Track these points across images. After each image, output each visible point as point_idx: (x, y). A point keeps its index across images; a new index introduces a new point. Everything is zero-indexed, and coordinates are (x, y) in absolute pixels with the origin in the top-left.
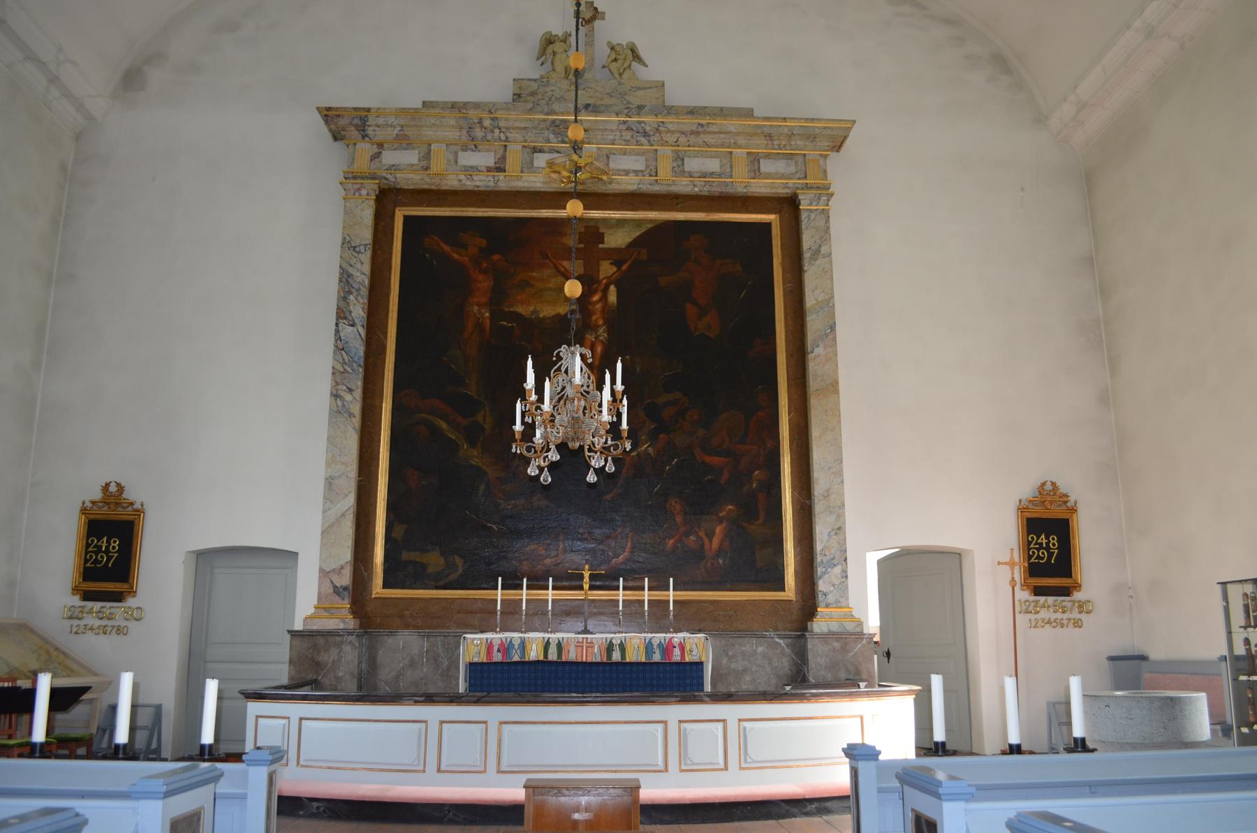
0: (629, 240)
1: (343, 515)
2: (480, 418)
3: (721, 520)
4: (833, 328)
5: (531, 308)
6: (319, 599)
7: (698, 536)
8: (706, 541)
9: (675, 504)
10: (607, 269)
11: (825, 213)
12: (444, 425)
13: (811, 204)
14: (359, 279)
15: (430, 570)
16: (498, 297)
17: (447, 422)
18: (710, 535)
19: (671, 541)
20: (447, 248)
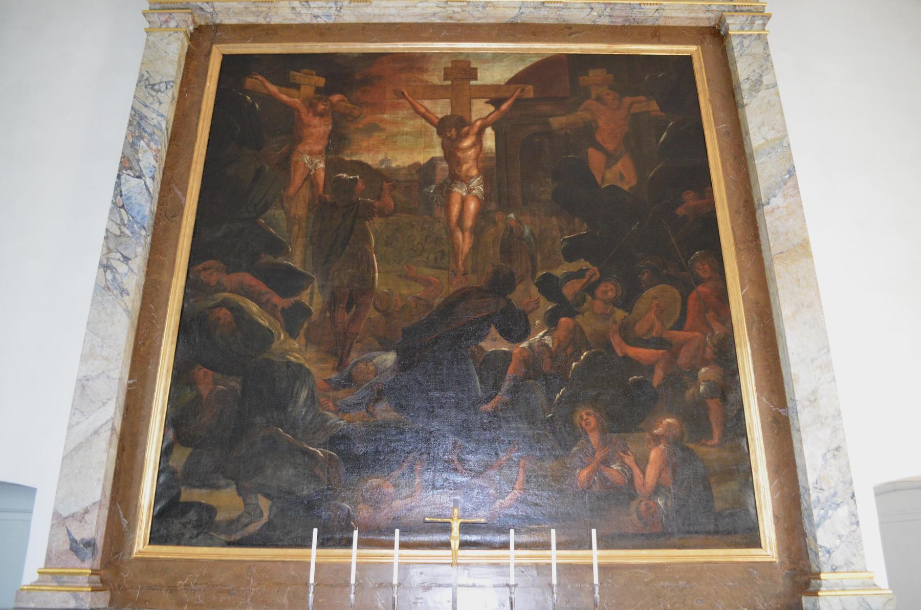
0: (509, 75)
1: (96, 432)
2: (304, 297)
3: (657, 439)
4: (791, 172)
5: (381, 157)
6: (48, 560)
7: (623, 464)
8: (637, 471)
9: (587, 417)
10: (481, 109)
11: (762, 38)
12: (254, 308)
13: (742, 29)
14: (155, 122)
15: (220, 517)
16: (338, 140)
17: (259, 303)
18: (642, 462)
19: (585, 472)
20: (273, 89)
